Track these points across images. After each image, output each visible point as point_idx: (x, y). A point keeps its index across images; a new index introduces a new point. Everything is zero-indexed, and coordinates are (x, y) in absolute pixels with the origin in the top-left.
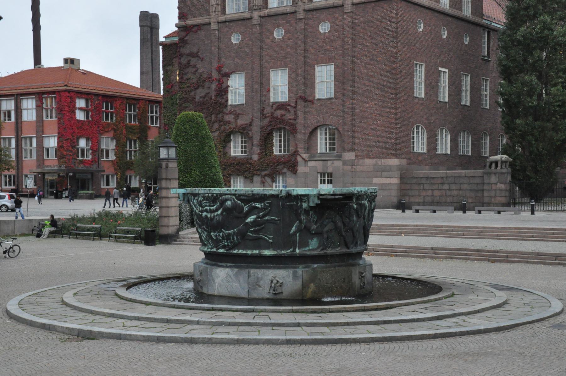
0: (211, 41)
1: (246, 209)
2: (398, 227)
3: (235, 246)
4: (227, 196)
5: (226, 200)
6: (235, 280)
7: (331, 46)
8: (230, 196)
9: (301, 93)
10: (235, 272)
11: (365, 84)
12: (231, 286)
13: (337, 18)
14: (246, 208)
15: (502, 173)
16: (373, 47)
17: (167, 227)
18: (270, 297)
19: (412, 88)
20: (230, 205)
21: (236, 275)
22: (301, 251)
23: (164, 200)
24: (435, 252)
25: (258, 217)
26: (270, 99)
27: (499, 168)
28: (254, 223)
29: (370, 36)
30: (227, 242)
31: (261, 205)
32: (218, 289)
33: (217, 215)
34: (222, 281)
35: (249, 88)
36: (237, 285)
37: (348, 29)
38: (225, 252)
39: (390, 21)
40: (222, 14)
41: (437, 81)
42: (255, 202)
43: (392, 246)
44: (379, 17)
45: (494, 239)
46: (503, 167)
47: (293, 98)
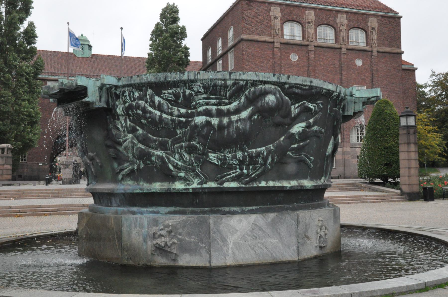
2: (50, 187)
4: (267, 86)
5: (266, 93)
8: (273, 87)
10: (269, 220)
12: (263, 244)
14: (295, 108)
15: (8, 157)
18: (317, 254)
20: (274, 101)
21: (273, 224)
25: (308, 126)
27: (5, 153)
28: (303, 135)
30: (248, 169)
32: (234, 254)
33: (237, 121)
34: (243, 237)
43: (40, 206)
46: (9, 153)
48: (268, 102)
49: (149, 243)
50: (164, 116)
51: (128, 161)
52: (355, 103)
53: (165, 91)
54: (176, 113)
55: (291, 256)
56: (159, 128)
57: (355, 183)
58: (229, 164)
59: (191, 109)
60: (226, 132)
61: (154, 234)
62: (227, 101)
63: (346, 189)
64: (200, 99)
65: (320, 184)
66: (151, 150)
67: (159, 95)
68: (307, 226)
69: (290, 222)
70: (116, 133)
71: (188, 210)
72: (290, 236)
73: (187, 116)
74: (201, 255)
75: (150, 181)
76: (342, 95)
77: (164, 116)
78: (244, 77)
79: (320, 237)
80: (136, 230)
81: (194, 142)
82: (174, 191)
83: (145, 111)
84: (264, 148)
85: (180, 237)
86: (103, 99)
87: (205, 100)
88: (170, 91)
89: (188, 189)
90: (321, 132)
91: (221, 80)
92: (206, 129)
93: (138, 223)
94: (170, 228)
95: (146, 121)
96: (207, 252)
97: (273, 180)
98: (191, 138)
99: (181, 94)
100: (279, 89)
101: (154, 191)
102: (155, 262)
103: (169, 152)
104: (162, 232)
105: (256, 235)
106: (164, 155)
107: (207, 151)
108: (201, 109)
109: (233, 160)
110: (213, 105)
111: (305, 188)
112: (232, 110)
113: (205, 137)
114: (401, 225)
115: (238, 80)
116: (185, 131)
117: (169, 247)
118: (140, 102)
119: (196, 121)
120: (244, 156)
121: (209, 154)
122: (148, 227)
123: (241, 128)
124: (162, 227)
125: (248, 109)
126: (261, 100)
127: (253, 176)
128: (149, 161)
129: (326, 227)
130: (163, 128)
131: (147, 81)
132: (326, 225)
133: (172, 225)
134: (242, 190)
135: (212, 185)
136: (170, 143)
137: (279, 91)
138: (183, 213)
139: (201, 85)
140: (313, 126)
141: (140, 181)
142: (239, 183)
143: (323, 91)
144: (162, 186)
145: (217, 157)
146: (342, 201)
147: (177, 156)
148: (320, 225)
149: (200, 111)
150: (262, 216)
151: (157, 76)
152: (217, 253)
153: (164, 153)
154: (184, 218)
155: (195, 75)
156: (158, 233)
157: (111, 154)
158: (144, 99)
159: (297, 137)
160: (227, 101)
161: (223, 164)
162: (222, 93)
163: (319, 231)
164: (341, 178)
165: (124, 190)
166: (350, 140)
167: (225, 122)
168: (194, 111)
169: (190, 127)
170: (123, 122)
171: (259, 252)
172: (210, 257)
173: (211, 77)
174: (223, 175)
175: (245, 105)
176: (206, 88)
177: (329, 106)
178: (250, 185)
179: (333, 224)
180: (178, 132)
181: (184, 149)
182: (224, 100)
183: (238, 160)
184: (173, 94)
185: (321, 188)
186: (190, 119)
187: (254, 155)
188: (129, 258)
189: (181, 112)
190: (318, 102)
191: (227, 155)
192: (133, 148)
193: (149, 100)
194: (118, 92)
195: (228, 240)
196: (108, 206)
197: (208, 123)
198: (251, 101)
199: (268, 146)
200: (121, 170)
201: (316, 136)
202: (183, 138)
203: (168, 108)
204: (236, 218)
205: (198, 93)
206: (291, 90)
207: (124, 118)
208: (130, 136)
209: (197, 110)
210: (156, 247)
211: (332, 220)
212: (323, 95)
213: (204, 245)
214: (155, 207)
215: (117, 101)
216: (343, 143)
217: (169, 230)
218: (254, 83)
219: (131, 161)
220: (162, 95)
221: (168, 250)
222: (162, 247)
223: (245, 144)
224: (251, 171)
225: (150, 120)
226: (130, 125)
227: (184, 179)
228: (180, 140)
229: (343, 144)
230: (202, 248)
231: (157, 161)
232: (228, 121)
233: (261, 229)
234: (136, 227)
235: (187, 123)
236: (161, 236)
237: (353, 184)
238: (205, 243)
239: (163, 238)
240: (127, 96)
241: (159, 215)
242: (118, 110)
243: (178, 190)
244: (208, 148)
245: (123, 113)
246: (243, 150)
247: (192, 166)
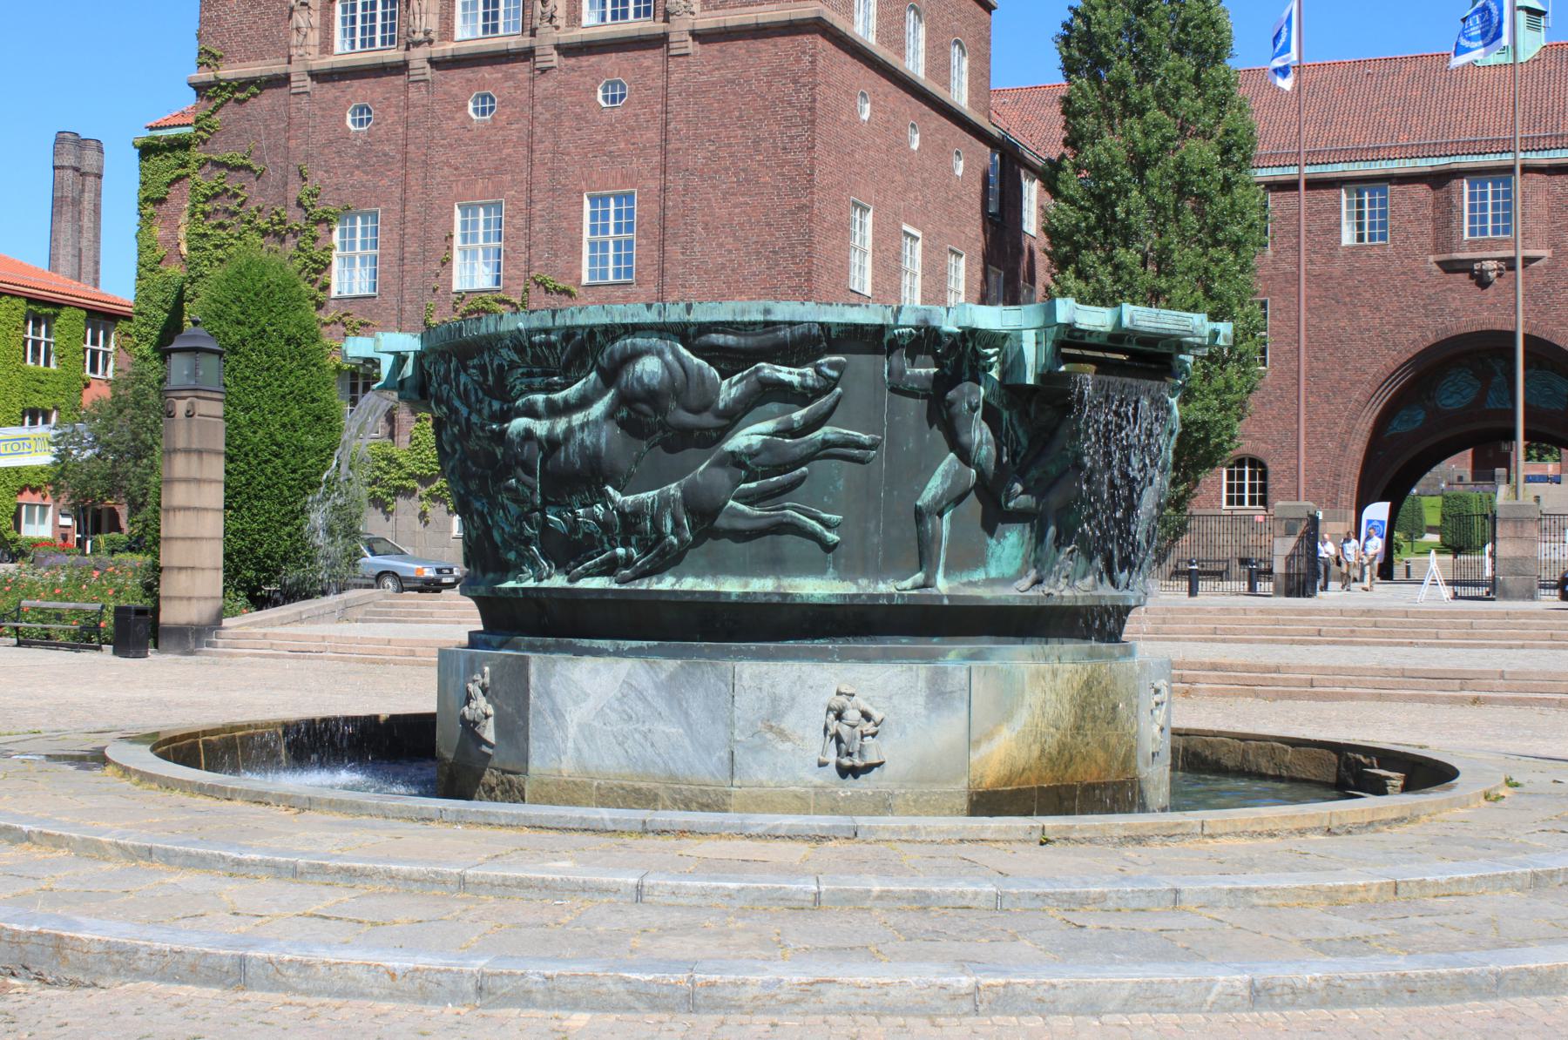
0: (289, 124)
1: (729, 391)
3: (667, 561)
5: (636, 355)
6: (666, 712)
7: (627, 142)
9: (541, 266)
10: (663, 676)
11: (721, 245)
13: (648, 68)
14: (730, 386)
16: (747, 147)
17: (185, 602)
19: (845, 267)
20: (654, 373)
21: (671, 688)
22: (955, 584)
23: (180, 516)
26: (450, 282)
29: (740, 118)
31: (803, 375)
32: (578, 750)
33: (582, 427)
34: (600, 713)
35: (392, 251)
36: (675, 730)
37: (677, 99)
38: (616, 586)
39: (795, 82)
40: (321, 52)
41: (898, 257)
42: (771, 359)
44: (764, 70)
47: (518, 281)
48: (641, 377)
55: (713, 775)
60: (563, 455)
72: (713, 723)
114: (272, 661)
123: (588, 443)
134: (610, 597)
171: (636, 754)
178: (643, 585)
179: (923, 712)
195: (567, 717)
198: (610, 376)
233: (641, 696)
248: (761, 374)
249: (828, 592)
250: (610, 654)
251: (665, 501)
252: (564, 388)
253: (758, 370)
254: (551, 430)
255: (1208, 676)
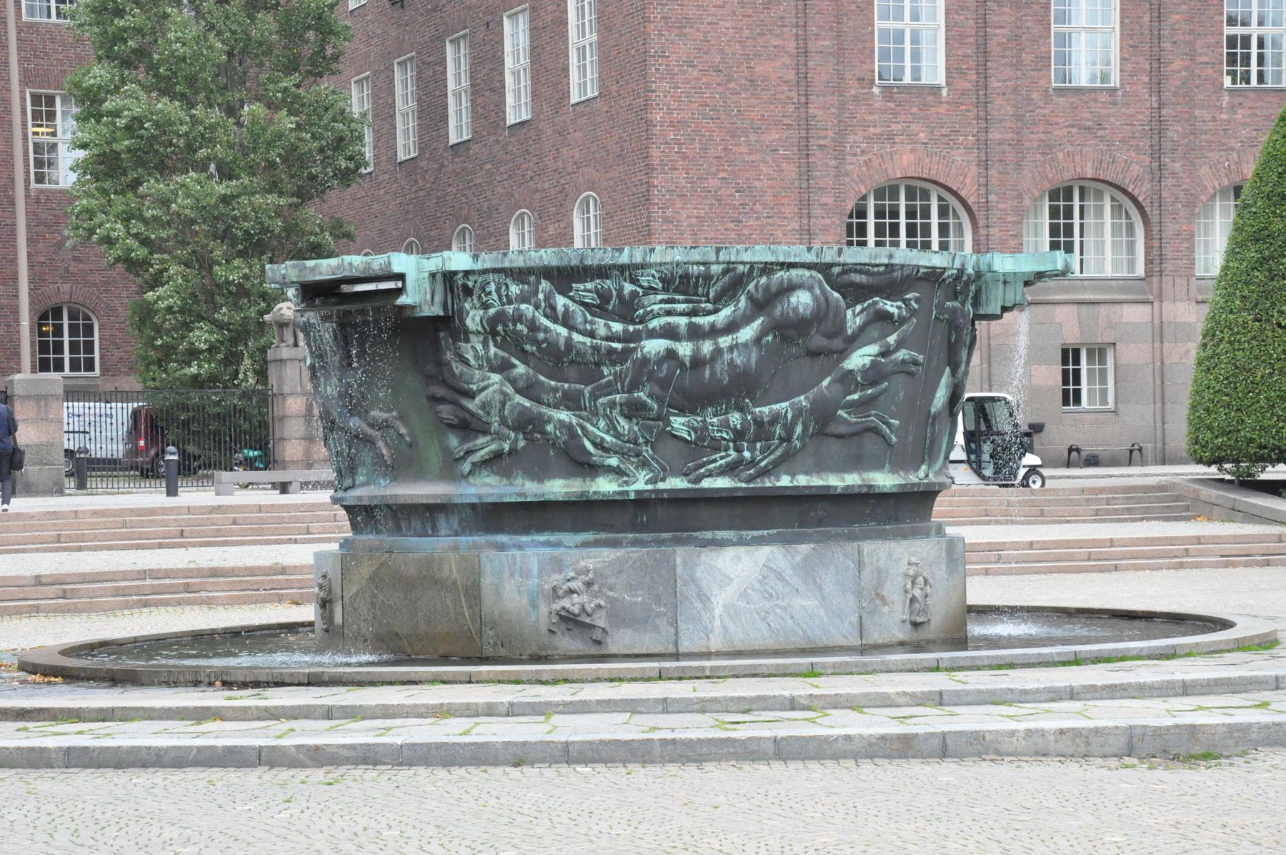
3: (785, 462)
5: (791, 288)
6: (802, 588)
8: (807, 273)
10: (799, 558)
14: (855, 316)
20: (808, 305)
21: (807, 569)
24: (65, 591)
25: (885, 353)
28: (874, 374)
30: (752, 450)
32: (725, 628)
33: (731, 349)
34: (744, 594)
45: (45, 550)
48: (797, 307)
49: (544, 610)
50: (577, 337)
51: (485, 432)
52: (1005, 283)
53: (578, 285)
54: (602, 331)
55: (845, 637)
56: (563, 363)
57: (1173, 486)
58: (713, 439)
59: (635, 323)
60: (707, 373)
61: (554, 589)
62: (709, 306)
63: (1129, 511)
64: (654, 303)
65: (915, 480)
66: (544, 410)
67: (564, 293)
68: (881, 577)
69: (843, 563)
70: (462, 371)
71: (626, 538)
72: (844, 594)
73: (626, 338)
74: (656, 629)
75: (540, 475)
76: (970, 270)
77: (577, 337)
78: (747, 257)
79: (913, 600)
80: (513, 581)
81: (641, 394)
82: (596, 497)
83: (533, 326)
84: (787, 404)
85: (611, 594)
86: (438, 298)
87: (663, 306)
88: (589, 285)
89: (627, 493)
90: (916, 363)
91: (698, 263)
92: (666, 366)
93: (518, 567)
94: (591, 575)
95: (534, 348)
96: (671, 624)
97: (806, 473)
98: (634, 386)
99: (615, 293)
100: (820, 276)
101: (552, 497)
102: (557, 649)
103: (584, 413)
104: (573, 585)
105: (770, 590)
106: (574, 421)
107: (668, 411)
108: (655, 324)
109: (721, 431)
110: (681, 314)
111: (877, 491)
112: (719, 325)
113: (664, 383)
115: (733, 263)
116: (622, 370)
117: (588, 615)
118: (523, 306)
119: (645, 350)
120: (744, 420)
121: (672, 418)
122: (540, 576)
124: (572, 574)
125: (753, 321)
126: (781, 302)
127: (763, 464)
128: (539, 432)
129: (926, 581)
130: (572, 362)
131: (541, 264)
132: (928, 577)
133: (595, 570)
134: (740, 494)
135: (677, 483)
136: (587, 395)
137: (820, 282)
138: (615, 544)
139: (657, 275)
140: (897, 349)
141: (516, 476)
142: (733, 480)
143: (918, 271)
144: (568, 486)
145: (688, 425)
146: (1089, 559)
147: (602, 424)
148: (911, 572)
149: (654, 329)
150: (783, 550)
151: (562, 254)
152: (690, 626)
153: (574, 415)
154: (618, 554)
155: (646, 254)
156: (565, 587)
157: (444, 415)
158: (532, 302)
159: (859, 379)
160: (709, 306)
161: (701, 438)
162: (700, 290)
163: (909, 586)
164: (1143, 463)
165: (479, 496)
166: (1192, 264)
167: (706, 351)
168: (640, 327)
169: (634, 362)
170: (479, 347)
171: (778, 627)
172: (677, 633)
173: (678, 258)
174: (700, 462)
175: (748, 313)
176: (667, 283)
177: (936, 301)
178: (758, 484)
179: (945, 575)
180: (606, 371)
181: (618, 408)
182: (703, 305)
183: (731, 429)
184: (597, 292)
185: (916, 490)
186: (632, 345)
187: (766, 420)
188: (499, 642)
189: (614, 330)
190: (908, 296)
191: (708, 420)
192: (503, 404)
193: (543, 304)
194: (470, 284)
196: (426, 535)
197: (671, 354)
198: (760, 305)
199: (796, 400)
200: (469, 453)
201: (903, 372)
202: (616, 384)
203: (586, 321)
204: (730, 552)
205: (651, 290)
206: (845, 277)
207: (481, 338)
208: (496, 377)
209: (647, 326)
210: (561, 616)
211: (943, 566)
212: (920, 279)
213: (662, 609)
214: (550, 533)
215: (465, 301)
216: (1155, 280)
217: (587, 579)
218: (767, 268)
219: (495, 433)
220: (571, 294)
221: (588, 620)
222: (575, 615)
223: (746, 396)
224: (758, 453)
225: (545, 345)
226: (496, 354)
227: (618, 472)
228: (609, 389)
229: (1155, 286)
230: (658, 615)
231: (558, 433)
232: (711, 348)
234: (512, 575)
235: (626, 354)
236: (571, 592)
237: (1161, 488)
238: (665, 606)
239: (575, 595)
240: (494, 293)
241: (562, 550)
242: (469, 322)
243: (604, 495)
244: (669, 406)
245: (480, 329)
246: (741, 409)
247: (636, 444)
248: (878, 307)
249: (892, 483)
250: (734, 544)
251: (798, 412)
252: (709, 313)
253: (875, 303)
254: (696, 351)
255: (218, 583)
